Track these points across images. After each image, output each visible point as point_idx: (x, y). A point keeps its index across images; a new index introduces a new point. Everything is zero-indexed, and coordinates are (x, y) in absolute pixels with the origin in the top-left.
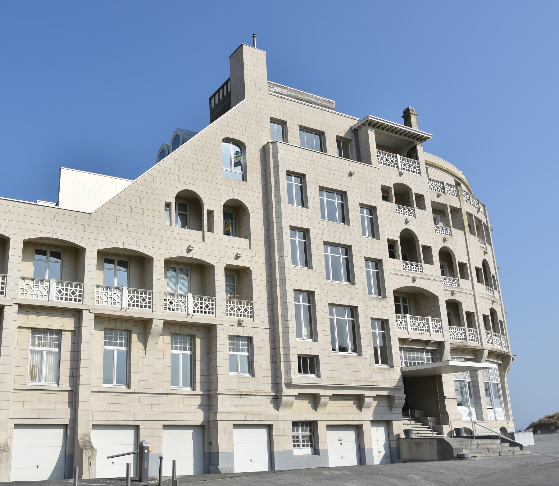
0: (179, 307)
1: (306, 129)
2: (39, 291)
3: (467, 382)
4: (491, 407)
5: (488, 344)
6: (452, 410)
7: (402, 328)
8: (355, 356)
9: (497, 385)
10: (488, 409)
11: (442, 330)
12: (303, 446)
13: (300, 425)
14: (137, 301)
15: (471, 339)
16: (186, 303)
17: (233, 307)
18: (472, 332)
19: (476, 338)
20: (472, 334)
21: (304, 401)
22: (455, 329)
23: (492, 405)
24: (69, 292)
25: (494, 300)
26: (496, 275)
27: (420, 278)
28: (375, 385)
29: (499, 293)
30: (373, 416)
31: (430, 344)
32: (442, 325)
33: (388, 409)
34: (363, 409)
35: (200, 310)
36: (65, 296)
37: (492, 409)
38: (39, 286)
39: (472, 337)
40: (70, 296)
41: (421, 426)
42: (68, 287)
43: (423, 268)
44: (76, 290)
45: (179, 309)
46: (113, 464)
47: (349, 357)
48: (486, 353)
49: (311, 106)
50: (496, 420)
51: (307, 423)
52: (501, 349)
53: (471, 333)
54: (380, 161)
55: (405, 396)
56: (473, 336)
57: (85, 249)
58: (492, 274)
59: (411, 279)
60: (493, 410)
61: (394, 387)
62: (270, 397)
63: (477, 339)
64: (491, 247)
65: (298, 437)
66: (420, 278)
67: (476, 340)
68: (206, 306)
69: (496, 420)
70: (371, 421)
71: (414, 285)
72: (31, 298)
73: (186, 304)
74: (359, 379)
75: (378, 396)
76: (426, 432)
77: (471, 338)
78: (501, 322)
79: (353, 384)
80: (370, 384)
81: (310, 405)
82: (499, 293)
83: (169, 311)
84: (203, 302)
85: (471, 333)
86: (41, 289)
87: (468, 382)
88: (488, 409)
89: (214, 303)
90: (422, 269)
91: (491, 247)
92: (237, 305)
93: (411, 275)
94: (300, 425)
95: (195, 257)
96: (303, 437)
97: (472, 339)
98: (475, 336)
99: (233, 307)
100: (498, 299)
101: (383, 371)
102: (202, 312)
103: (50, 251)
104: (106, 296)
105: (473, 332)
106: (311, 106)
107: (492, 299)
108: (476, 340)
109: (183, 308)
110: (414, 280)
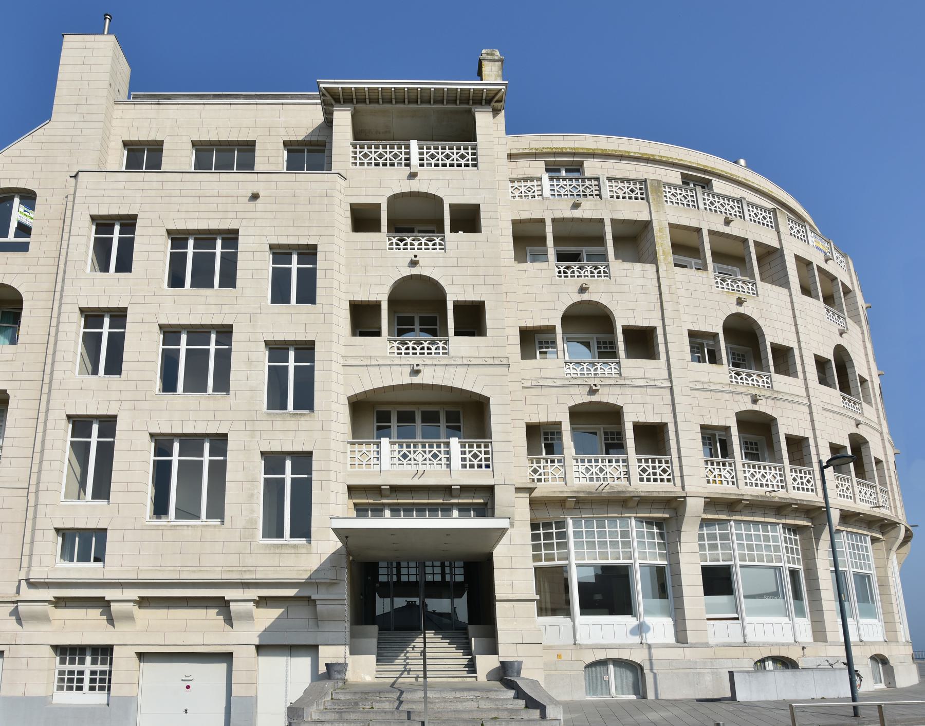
0: (723, 479)
1: (215, 145)
2: (580, 473)
3: (852, 573)
4: (736, 616)
5: (862, 503)
6: (515, 623)
7: (730, 483)
8: (219, 526)
9: (869, 577)
10: (708, 619)
11: (737, 480)
12: (92, 689)
13: (88, 652)
14: (655, 474)
15: (840, 494)
16: (733, 471)
17: (796, 477)
18: (841, 481)
19: (850, 493)
20: (842, 484)
21: (89, 611)
22: (841, 479)
23: (737, 612)
24: (658, 471)
25: (861, 419)
26: (871, 376)
27: (767, 397)
28: (248, 577)
29: (877, 410)
30: (260, 636)
31: (740, 507)
32: (785, 475)
33: (311, 622)
34: (116, 624)
35: (800, 486)
36: (657, 478)
37: (737, 619)
38: (580, 466)
39: (843, 490)
40: (660, 475)
41: (463, 655)
42: (592, 463)
43: (773, 380)
44: (648, 467)
45: (723, 481)
46: (186, 713)
47: (186, 528)
48: (835, 516)
49: (202, 104)
50: (746, 643)
51: (108, 648)
52: (877, 510)
53: (840, 482)
54: (753, 219)
55: (538, 597)
56: (845, 488)
57: (774, 420)
58: (860, 376)
59: (750, 398)
60: (740, 622)
61: (304, 581)
62: (11, 605)
63: (852, 495)
64: (861, 327)
65: (93, 673)
66: (767, 397)
67: (850, 496)
68: (807, 481)
69: (745, 642)
70: (255, 645)
71: (756, 408)
72: (620, 483)
73: (733, 474)
74: (205, 568)
75: (261, 598)
76: (449, 668)
77: (840, 491)
78: (878, 462)
79: (186, 576)
80: (234, 576)
81: (105, 617)
82: (877, 410)
83: (714, 485)
84: (803, 475)
85: (840, 482)
86: (582, 469)
87: (789, 570)
88: (708, 619)
89: (782, 473)
90: (771, 382)
91: (861, 327)
92: (760, 471)
93: (749, 392)
94: (88, 652)
95: (762, 410)
96: (81, 673)
97: (842, 493)
98: (847, 489)
99: (796, 477)
100: (876, 420)
101: (277, 551)
102: (803, 489)
103: (398, 411)
104: (403, 464)
105: (845, 482)
106: (202, 104)
107: (858, 417)
108: (850, 496)
109: (730, 479)
110: (755, 401)
